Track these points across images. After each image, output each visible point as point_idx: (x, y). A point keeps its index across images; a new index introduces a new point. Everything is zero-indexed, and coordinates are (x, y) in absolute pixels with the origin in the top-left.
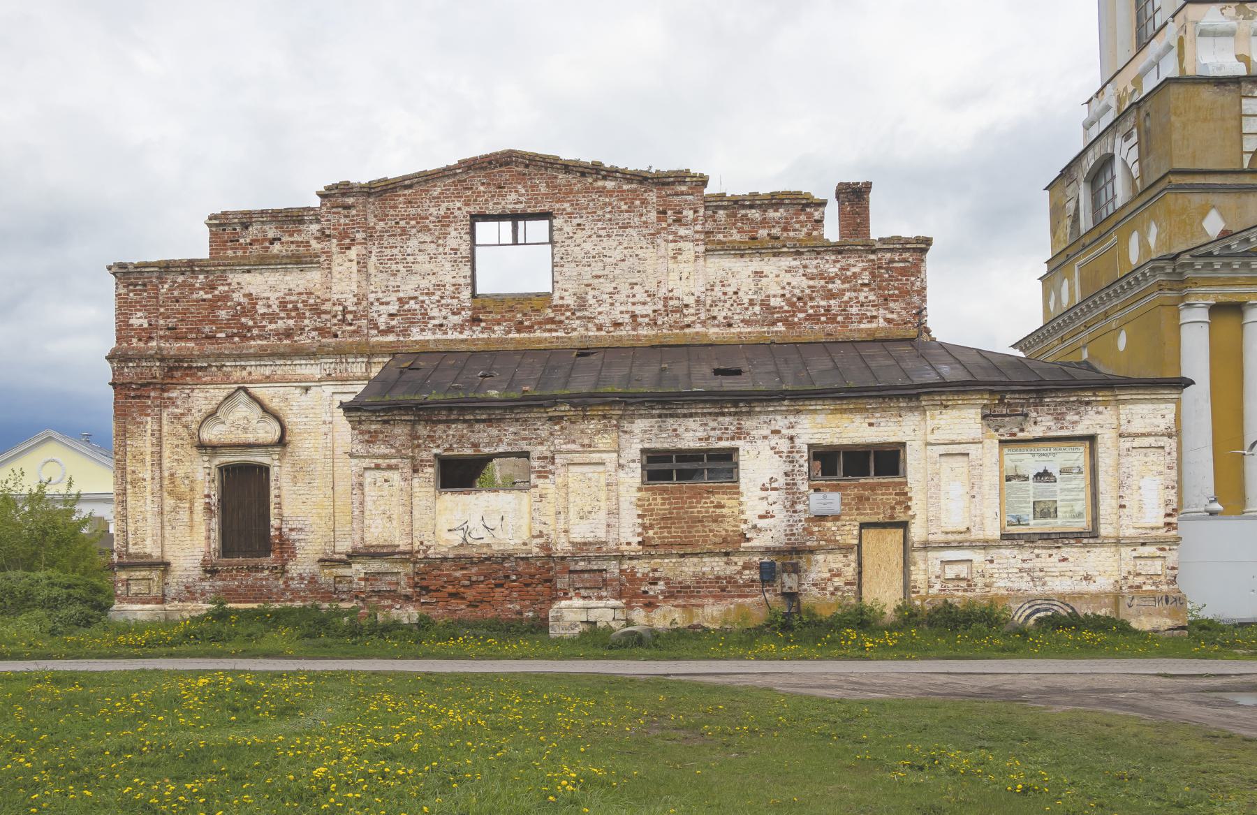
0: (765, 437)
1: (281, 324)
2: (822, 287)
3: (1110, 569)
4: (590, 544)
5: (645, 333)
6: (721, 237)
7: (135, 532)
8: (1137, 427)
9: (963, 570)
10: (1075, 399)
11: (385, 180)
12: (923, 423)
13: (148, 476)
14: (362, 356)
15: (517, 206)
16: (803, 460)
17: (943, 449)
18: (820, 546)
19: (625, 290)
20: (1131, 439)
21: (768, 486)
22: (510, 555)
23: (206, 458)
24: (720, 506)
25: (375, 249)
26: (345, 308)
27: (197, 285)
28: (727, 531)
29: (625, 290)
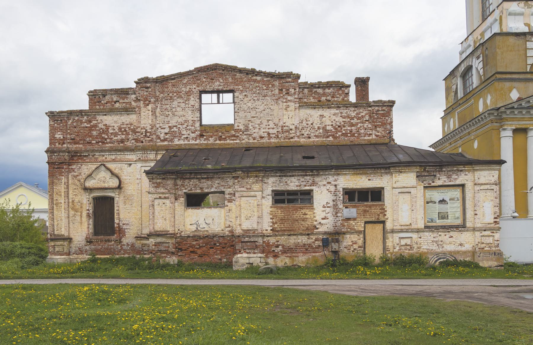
0: (324, 185)
1: (119, 137)
2: (349, 121)
4: (250, 230)
5: (273, 141)
6: (306, 100)
7: (57, 225)
8: (482, 181)
9: (408, 241)
10: (456, 169)
11: (163, 76)
12: (391, 179)
13: (63, 201)
14: (154, 151)
15: (219, 87)
17: (400, 190)
19: (265, 123)
21: (326, 206)
22: (216, 235)
23: (87, 194)
24: (305, 214)
25: (159, 106)
26: (146, 130)
27: (84, 121)
28: (308, 225)
29: (265, 123)
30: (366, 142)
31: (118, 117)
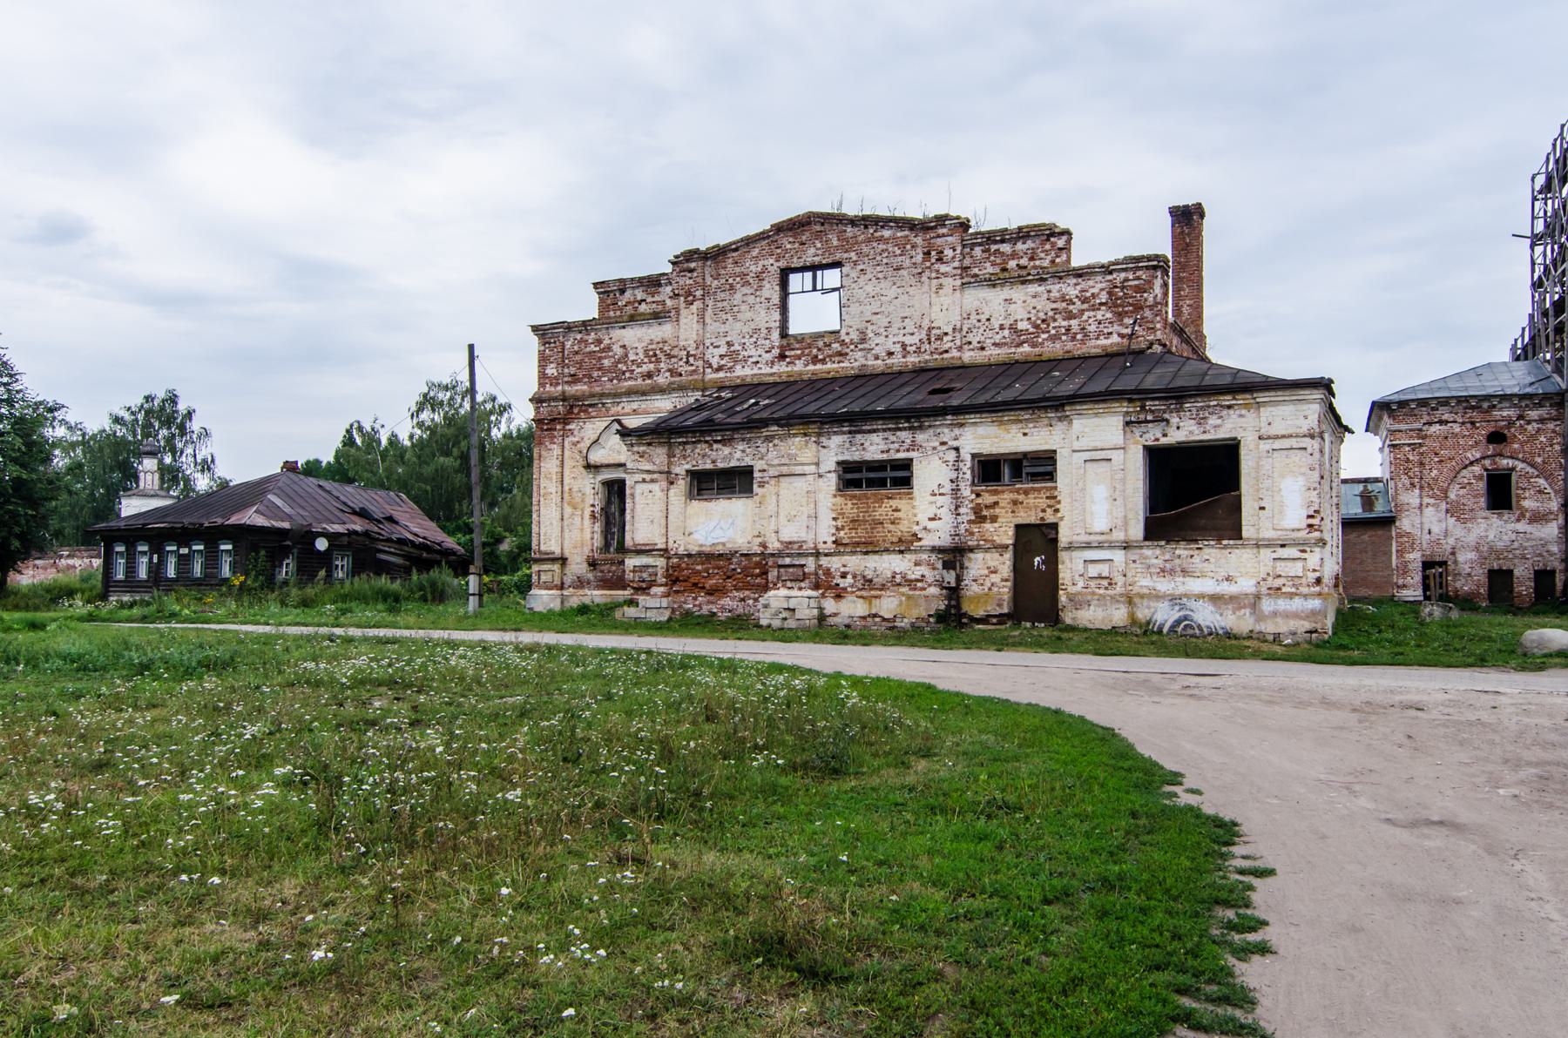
1: (645, 368)
2: (1065, 309)
3: (1253, 570)
4: (794, 543)
5: (912, 359)
6: (976, 271)
7: (545, 535)
8: (1278, 429)
9: (1104, 569)
10: (1215, 403)
11: (718, 246)
13: (554, 490)
14: (698, 390)
15: (815, 259)
16: (966, 467)
17: (1088, 455)
18: (978, 545)
19: (897, 324)
20: (1271, 441)
21: (936, 492)
22: (736, 552)
23: (591, 476)
24: (897, 510)
25: (710, 303)
26: (688, 352)
27: (590, 341)
29: (897, 324)
30: (1099, 351)
31: (644, 330)
